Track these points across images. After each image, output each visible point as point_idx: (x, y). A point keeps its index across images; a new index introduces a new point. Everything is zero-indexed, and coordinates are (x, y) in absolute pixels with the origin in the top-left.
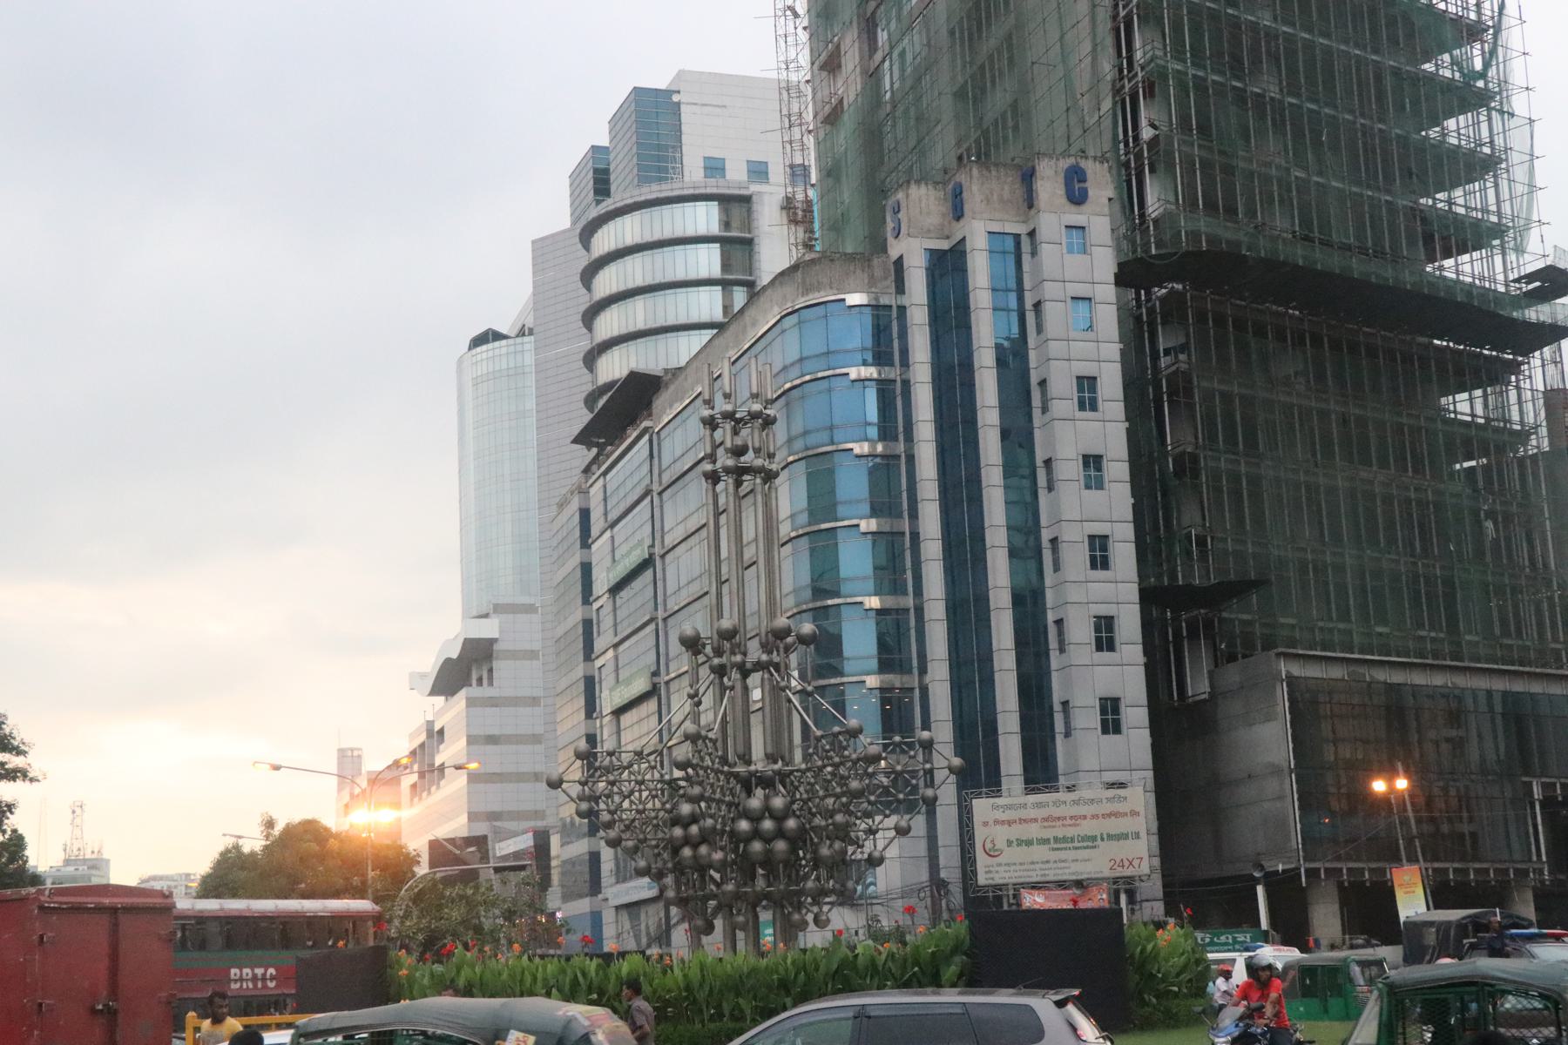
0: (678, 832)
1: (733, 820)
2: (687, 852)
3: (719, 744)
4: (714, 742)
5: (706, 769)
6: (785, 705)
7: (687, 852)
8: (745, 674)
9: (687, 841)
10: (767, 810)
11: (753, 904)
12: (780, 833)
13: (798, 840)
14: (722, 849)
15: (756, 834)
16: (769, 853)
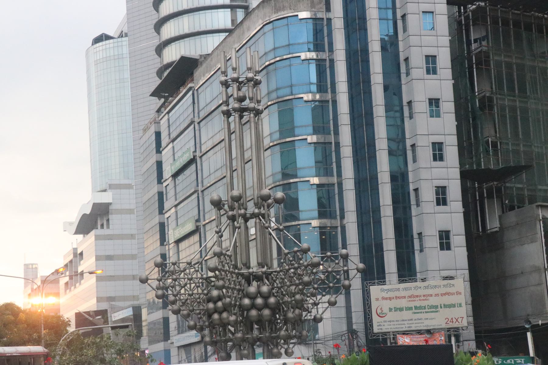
0: (211, 305)
1: (241, 299)
2: (216, 316)
3: (233, 258)
4: (230, 256)
5: (225, 271)
7: (216, 316)
8: (246, 220)
9: (216, 310)
10: (259, 293)
12: (266, 305)
13: (276, 309)
14: (235, 314)
15: (253, 306)
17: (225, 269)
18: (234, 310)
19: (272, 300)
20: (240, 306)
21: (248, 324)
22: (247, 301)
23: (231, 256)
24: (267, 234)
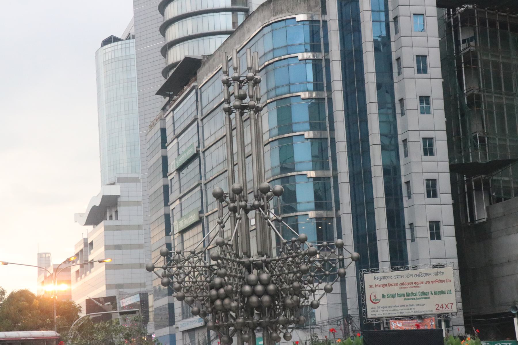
0: (214, 292)
1: (242, 286)
2: (218, 302)
3: (234, 247)
4: (231, 246)
5: (227, 260)
6: (267, 226)
7: (218, 302)
8: (247, 211)
9: (218, 297)
10: (259, 281)
11: (253, 329)
13: (275, 296)
15: (254, 293)
17: (227, 257)
18: (236, 296)
19: (271, 287)
20: (241, 293)
21: (249, 310)
22: (247, 288)
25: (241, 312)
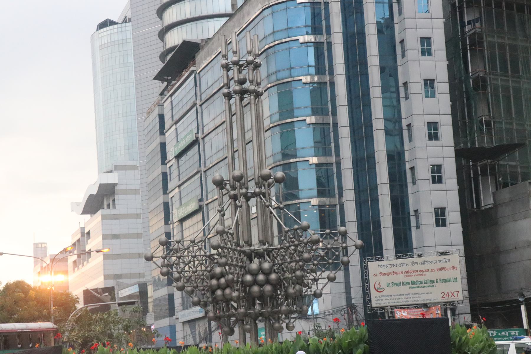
0: (214, 282)
1: (243, 275)
3: (235, 236)
4: (232, 234)
6: (269, 215)
7: (219, 292)
8: (248, 199)
9: (219, 287)
10: (261, 270)
12: (268, 282)
13: (277, 285)
14: (237, 290)
15: (255, 282)
16: (262, 292)
17: (228, 246)
18: (237, 286)
19: (273, 276)
23: (233, 234)
24: (268, 212)
25: (243, 302)
